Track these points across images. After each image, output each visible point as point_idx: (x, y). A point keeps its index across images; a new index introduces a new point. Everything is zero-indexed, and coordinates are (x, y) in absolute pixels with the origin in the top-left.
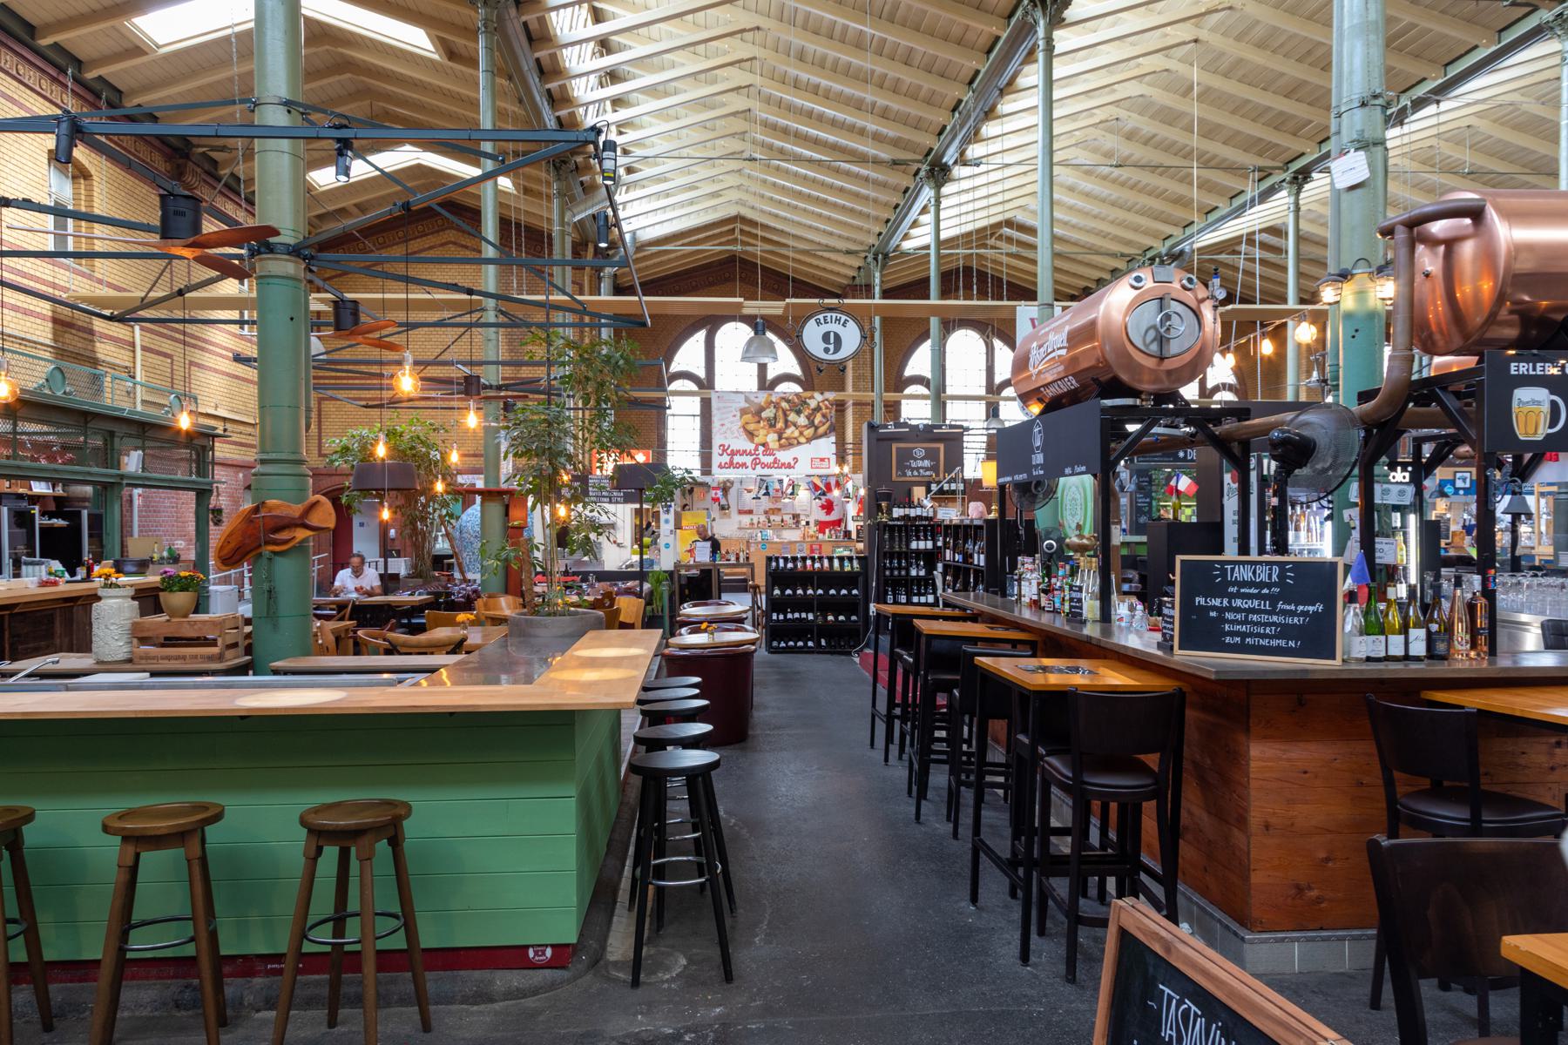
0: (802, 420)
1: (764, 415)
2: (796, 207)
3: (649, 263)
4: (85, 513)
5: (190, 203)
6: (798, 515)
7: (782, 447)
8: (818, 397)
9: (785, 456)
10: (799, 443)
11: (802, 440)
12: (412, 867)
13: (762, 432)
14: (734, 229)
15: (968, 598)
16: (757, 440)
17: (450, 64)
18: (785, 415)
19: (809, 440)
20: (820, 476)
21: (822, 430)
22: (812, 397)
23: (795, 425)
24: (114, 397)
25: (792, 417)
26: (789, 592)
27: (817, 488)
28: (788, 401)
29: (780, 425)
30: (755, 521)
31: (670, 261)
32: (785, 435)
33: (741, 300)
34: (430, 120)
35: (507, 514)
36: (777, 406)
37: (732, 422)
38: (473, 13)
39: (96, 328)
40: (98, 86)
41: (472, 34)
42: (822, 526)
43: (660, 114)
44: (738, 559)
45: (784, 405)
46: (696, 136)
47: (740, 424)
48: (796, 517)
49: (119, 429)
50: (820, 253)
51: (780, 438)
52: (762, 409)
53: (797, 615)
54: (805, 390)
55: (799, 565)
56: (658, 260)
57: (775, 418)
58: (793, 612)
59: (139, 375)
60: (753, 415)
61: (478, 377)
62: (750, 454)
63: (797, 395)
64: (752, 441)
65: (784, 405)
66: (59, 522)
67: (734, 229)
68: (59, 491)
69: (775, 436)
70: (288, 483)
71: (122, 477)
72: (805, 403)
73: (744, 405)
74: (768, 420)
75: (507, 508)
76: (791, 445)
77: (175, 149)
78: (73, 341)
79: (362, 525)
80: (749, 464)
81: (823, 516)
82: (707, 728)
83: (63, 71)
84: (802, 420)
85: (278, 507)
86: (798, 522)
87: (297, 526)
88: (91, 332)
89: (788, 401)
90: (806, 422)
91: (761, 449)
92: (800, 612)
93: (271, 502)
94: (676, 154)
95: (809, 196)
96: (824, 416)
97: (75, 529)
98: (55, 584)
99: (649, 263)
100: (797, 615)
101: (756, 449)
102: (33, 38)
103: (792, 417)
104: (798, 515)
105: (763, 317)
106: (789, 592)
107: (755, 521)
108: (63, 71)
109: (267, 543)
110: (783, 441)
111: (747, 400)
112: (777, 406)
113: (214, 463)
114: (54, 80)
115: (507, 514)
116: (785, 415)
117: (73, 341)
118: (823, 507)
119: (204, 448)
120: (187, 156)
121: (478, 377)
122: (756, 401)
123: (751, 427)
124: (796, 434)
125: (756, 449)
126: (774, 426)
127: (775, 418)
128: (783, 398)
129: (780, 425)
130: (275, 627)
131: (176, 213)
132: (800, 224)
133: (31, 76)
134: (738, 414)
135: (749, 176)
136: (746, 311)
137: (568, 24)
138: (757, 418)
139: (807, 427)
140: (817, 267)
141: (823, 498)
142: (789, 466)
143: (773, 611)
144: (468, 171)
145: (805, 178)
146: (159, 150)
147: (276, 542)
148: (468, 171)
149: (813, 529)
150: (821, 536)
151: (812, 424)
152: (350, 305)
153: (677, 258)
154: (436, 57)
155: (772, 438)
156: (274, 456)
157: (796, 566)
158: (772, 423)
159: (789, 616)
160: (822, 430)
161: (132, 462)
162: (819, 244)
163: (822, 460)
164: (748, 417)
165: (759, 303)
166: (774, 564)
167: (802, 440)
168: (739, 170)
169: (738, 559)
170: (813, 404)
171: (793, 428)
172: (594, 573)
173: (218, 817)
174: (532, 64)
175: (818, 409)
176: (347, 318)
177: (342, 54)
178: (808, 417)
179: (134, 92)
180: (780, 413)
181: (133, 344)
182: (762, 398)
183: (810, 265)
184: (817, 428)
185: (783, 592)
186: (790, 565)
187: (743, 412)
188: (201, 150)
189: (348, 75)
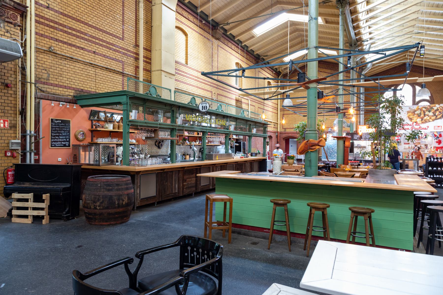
0: (431, 114)
1: (416, 113)
2: (431, 45)
3: (375, 69)
4: (242, 142)
5: (304, 74)
6: (427, 145)
7: (422, 123)
8: (437, 106)
9: (424, 126)
10: (429, 121)
11: (431, 120)
12: (374, 226)
13: (415, 118)
14: (406, 55)
15: (394, 184)
16: (413, 121)
17: (327, 25)
18: (424, 112)
19: (433, 120)
20: (436, 132)
21: (438, 117)
22: (435, 106)
23: (428, 115)
24: (248, 115)
25: (427, 113)
26: (435, 169)
27: (435, 136)
28: (425, 108)
29: (422, 116)
30: (410, 147)
31: (382, 68)
32: (424, 119)
33: (417, 78)
34: (325, 41)
35: (344, 143)
36: (421, 110)
37: (404, 116)
38: (338, 11)
39: (242, 101)
40: (244, 47)
41: (338, 16)
42: (437, 148)
43: (387, 25)
44: (412, 158)
45: (424, 109)
46: (397, 29)
47: (407, 116)
48: (426, 145)
49: (252, 124)
50: (439, 59)
51: (422, 120)
52: (415, 111)
53: (438, 176)
54: (431, 104)
55: (439, 160)
56: (378, 68)
57: (420, 114)
58: (436, 175)
59: (250, 111)
60: (412, 113)
61: (340, 107)
62: (411, 125)
63: (429, 106)
64: (411, 121)
65: (424, 109)
66: (237, 144)
67: (406, 55)
68: (237, 138)
69: (420, 119)
70: (314, 135)
71: (252, 134)
72: (432, 108)
73: (408, 110)
74: (418, 114)
75: (344, 142)
76: (426, 122)
77: (257, 58)
78: (239, 104)
79: (292, 146)
80: (410, 128)
81: (437, 145)
82: (428, 207)
83: (239, 45)
84: (431, 114)
85: (312, 141)
86: (427, 147)
87: (317, 145)
88: (241, 102)
89: (425, 108)
90: (433, 114)
91: (415, 124)
92: (439, 175)
93: (310, 140)
94: (388, 36)
95: (437, 41)
96: (440, 112)
97: (240, 146)
98: (243, 158)
99: (375, 69)
100: (438, 176)
101: (413, 124)
102: (234, 39)
103: (427, 113)
104: (427, 145)
105: (424, 82)
106: (435, 169)
107: (410, 147)
108: (239, 45)
109: (310, 149)
110: (423, 121)
111: (410, 108)
112: (421, 110)
113: (267, 132)
114: (237, 47)
115: (344, 143)
116: (424, 112)
117: (239, 104)
118: (437, 142)
119: (265, 127)
120: (259, 59)
121: (340, 107)
122: (413, 108)
123: (411, 117)
124: (429, 118)
125: (413, 124)
126: (420, 116)
127: (420, 114)
128: (424, 107)
129: (422, 116)
130: (311, 168)
131: (302, 77)
132: (432, 50)
133: (233, 47)
134: (406, 113)
135: (414, 38)
136: (418, 81)
137: (361, 7)
138: (413, 114)
139: (433, 116)
140: (437, 63)
141: (438, 139)
142: (425, 129)
143: (429, 174)
144: (334, 53)
145: (437, 35)
146: (254, 58)
147: (312, 149)
148: (334, 53)
149: (433, 150)
150: (436, 152)
151: (435, 115)
152: (321, 92)
153: (385, 67)
154: (323, 23)
155: (419, 120)
156: (311, 129)
157: (438, 161)
158: (419, 115)
159: (435, 176)
160: (438, 117)
161: (254, 131)
162: (439, 55)
163: (439, 127)
164: (410, 114)
165: (424, 78)
166: (429, 160)
167: (431, 120)
168: (411, 37)
169: (412, 158)
170: (435, 108)
171: (427, 117)
172: (364, 160)
173: (329, 207)
174: (351, 19)
175: (437, 110)
176: (321, 95)
177: (296, 28)
178: (433, 113)
179: (251, 46)
180: (422, 112)
181: (248, 104)
182: (415, 107)
183: (435, 63)
184: (437, 116)
185: (433, 168)
186: (436, 160)
187: (408, 112)
188: (262, 57)
189: (297, 32)
